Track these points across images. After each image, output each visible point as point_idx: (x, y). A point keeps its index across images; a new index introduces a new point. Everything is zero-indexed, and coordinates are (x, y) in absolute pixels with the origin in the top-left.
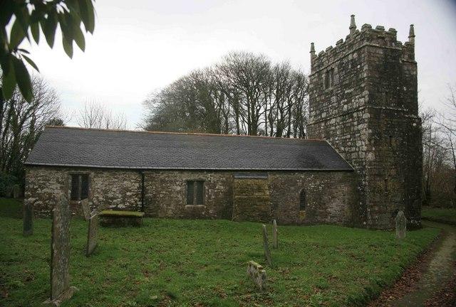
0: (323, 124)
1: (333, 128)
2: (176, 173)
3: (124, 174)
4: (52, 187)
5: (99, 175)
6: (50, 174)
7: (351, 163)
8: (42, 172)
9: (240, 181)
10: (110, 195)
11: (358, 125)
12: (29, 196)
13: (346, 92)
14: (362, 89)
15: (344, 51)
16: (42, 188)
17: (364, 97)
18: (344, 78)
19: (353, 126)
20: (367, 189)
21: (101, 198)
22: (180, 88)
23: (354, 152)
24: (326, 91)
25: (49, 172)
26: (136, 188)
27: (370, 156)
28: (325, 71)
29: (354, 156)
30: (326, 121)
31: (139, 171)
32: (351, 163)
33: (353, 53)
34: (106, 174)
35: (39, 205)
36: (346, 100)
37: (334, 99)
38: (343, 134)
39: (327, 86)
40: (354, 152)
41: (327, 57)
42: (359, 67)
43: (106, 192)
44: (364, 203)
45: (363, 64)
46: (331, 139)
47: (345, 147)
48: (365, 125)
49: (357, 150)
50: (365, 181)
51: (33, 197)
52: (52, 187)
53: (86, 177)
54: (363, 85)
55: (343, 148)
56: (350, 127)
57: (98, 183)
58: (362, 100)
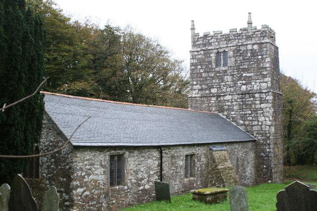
0: (214, 99)
1: (229, 104)
2: (181, 148)
3: (148, 151)
4: (96, 172)
5: (132, 154)
6: (94, 156)
7: (253, 135)
8: (88, 155)
9: (220, 153)
10: (140, 176)
11: (260, 104)
12: (77, 187)
13: (244, 75)
14: (264, 76)
15: (239, 39)
16: (89, 175)
17: (267, 82)
18: (241, 62)
19: (255, 104)
20: (272, 155)
21: (133, 181)
22: (148, 65)
23: (255, 125)
24: (217, 69)
25: (93, 154)
26: (156, 165)
27: (273, 129)
28: (215, 51)
29: (255, 128)
30: (218, 96)
31: (159, 148)
32: (253, 135)
33: (254, 44)
34: (136, 152)
35: (87, 196)
36: (244, 82)
37: (228, 78)
38: (241, 109)
39: (218, 65)
40: (255, 125)
41: (217, 39)
42: (260, 57)
43: (136, 172)
44: (269, 166)
45: (264, 56)
46: (226, 113)
47: (244, 121)
48: (270, 105)
49: (260, 123)
50: (270, 148)
51: (82, 187)
52: (96, 172)
53: (120, 157)
54: (265, 73)
55: (241, 122)
56: (251, 105)
57: (131, 163)
58: (264, 84)
